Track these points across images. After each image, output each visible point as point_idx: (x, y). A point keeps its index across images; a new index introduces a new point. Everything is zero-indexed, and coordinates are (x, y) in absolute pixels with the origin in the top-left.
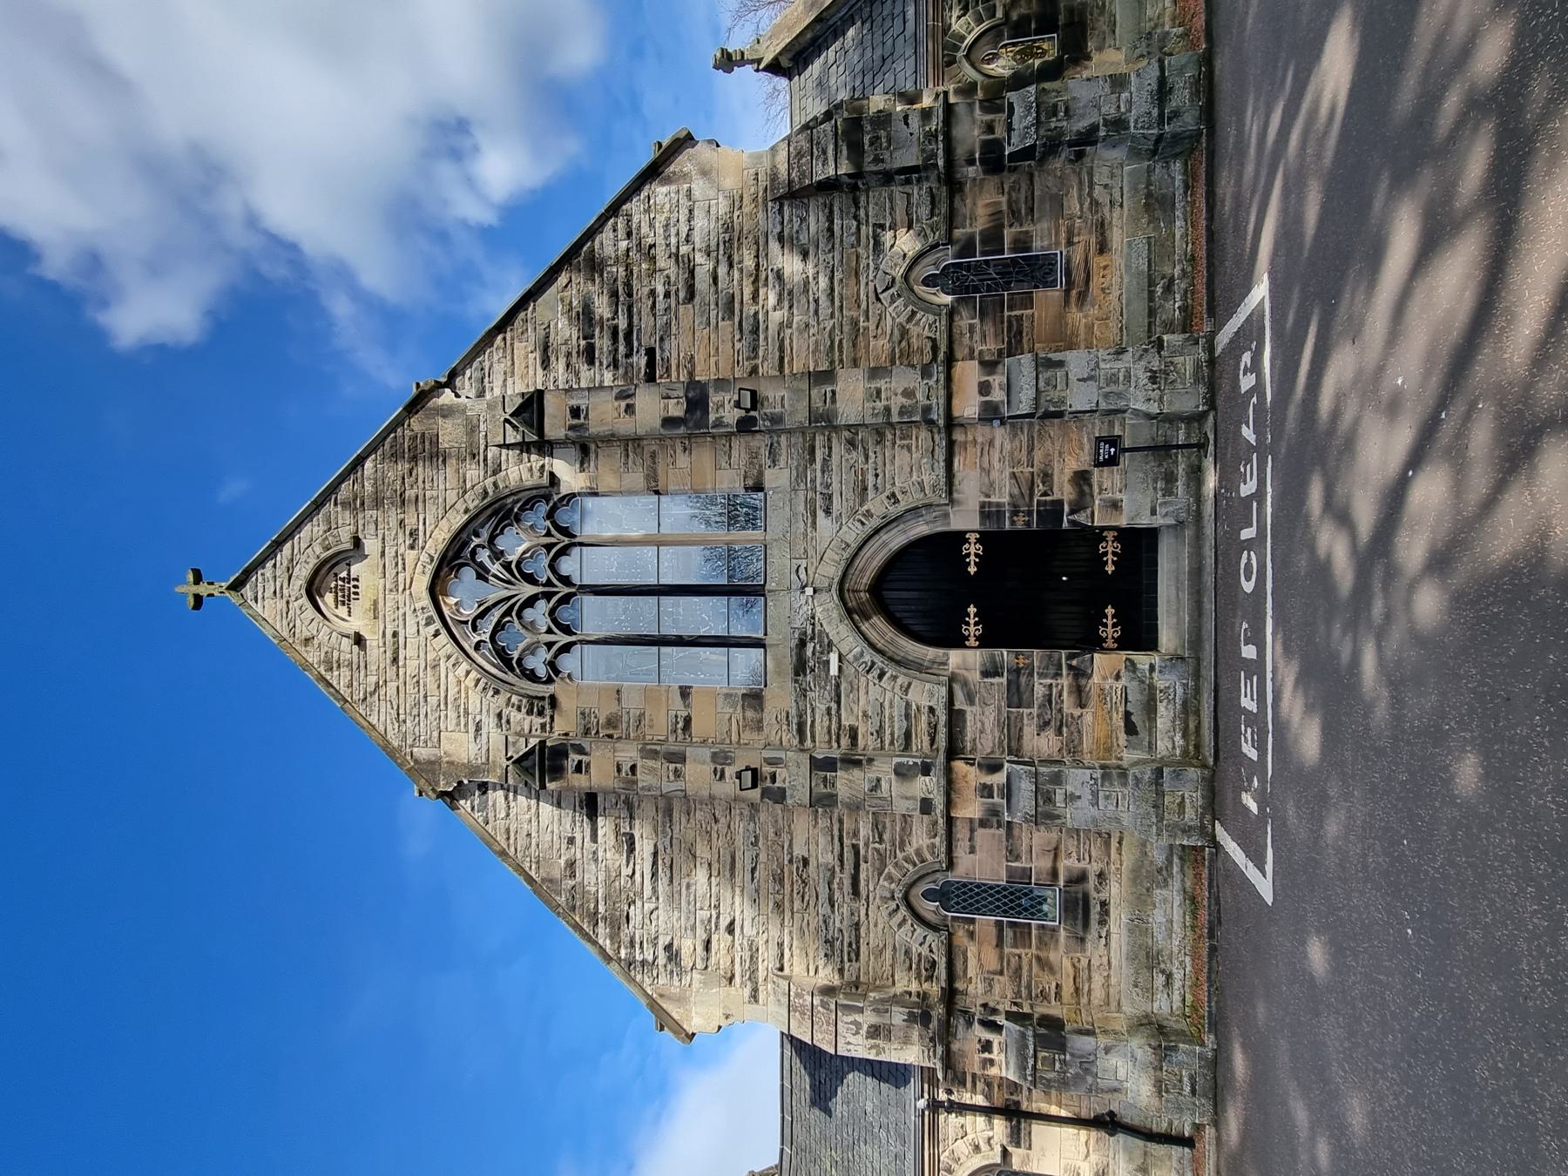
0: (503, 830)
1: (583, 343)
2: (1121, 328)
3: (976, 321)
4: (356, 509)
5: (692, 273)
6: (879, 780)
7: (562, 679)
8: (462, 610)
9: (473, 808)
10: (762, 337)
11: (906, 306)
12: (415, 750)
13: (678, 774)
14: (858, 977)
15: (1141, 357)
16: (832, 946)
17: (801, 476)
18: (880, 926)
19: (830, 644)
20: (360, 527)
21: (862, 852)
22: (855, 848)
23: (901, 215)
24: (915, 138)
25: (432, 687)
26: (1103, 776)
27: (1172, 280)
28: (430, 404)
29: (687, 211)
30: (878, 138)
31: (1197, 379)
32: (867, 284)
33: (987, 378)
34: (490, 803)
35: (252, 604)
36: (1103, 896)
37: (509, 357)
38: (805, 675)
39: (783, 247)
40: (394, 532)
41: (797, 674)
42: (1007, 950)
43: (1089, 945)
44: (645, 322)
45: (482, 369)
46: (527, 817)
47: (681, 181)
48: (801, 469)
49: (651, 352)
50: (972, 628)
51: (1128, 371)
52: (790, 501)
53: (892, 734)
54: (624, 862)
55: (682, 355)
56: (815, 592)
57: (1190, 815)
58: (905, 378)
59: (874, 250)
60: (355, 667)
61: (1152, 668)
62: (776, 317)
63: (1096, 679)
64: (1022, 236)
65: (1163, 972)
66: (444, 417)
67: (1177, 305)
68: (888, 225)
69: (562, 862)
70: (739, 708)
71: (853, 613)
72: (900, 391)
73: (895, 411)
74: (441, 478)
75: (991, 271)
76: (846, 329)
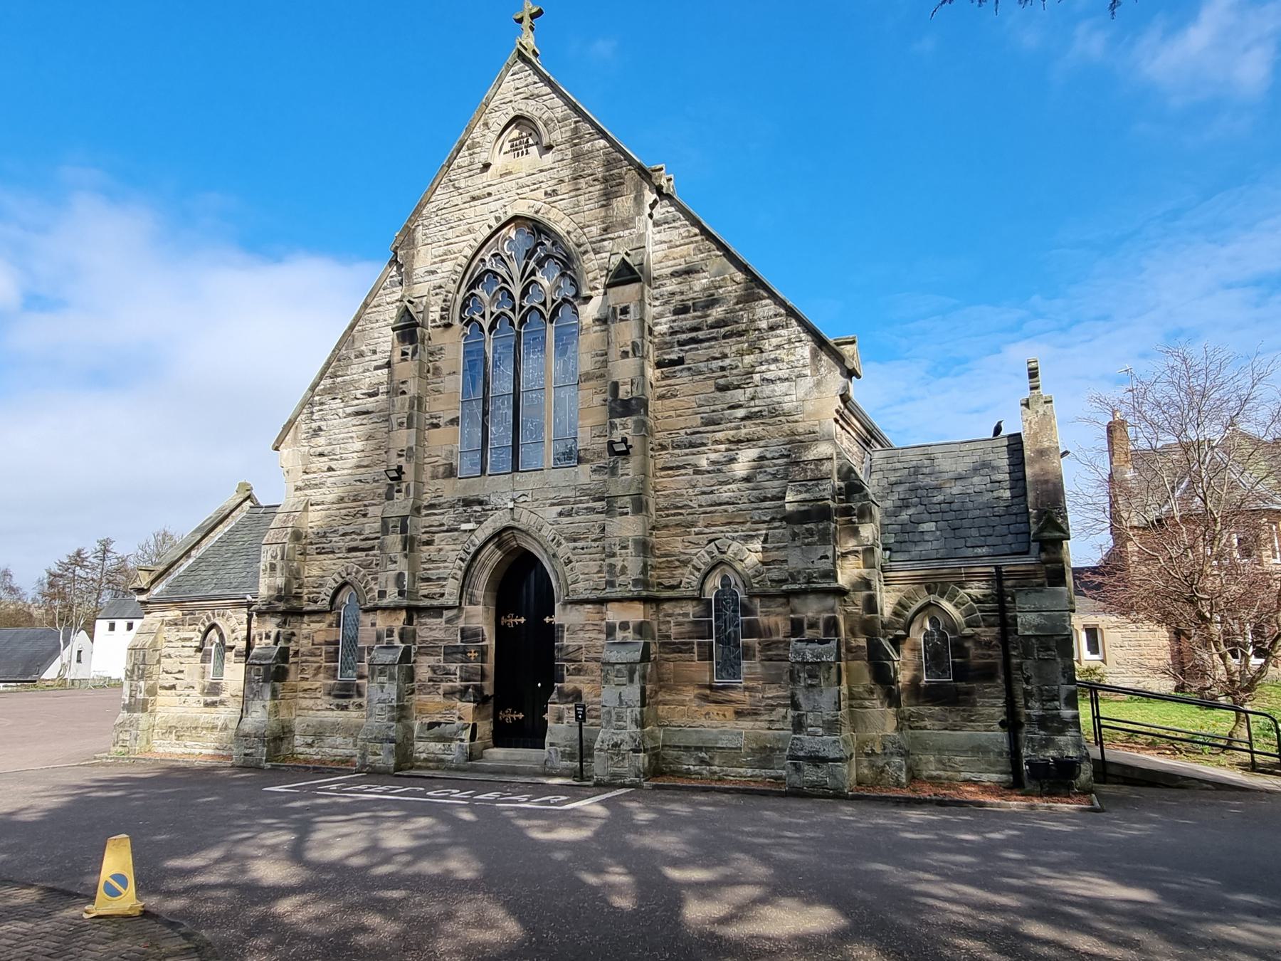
0: (379, 302)
1: (690, 303)
2: (680, 726)
3: (691, 618)
4: (573, 139)
5: (738, 387)
6: (395, 562)
7: (463, 329)
8: (507, 242)
9: (392, 277)
10: (687, 451)
11: (704, 563)
12: (421, 227)
13: (401, 424)
14: (308, 554)
15: (632, 737)
16: (323, 537)
17: (584, 492)
18: (333, 567)
19: (480, 523)
20: (559, 147)
21: (371, 553)
22: (372, 548)
23: (773, 556)
24: (810, 565)
25: (458, 231)
26: (393, 706)
27: (710, 765)
28: (645, 184)
29: (786, 376)
30: (812, 535)
31: (614, 775)
32: (722, 532)
33: (631, 627)
34: (394, 289)
35: (511, 73)
36: (351, 707)
37: (682, 242)
38: (463, 506)
39: (754, 461)
40: (556, 176)
41: (464, 500)
42: (323, 647)
43: (327, 698)
44: (702, 352)
45: (674, 221)
46: (387, 318)
47: (813, 367)
48: (588, 492)
49: (680, 361)
50: (511, 621)
51: (625, 728)
52: (569, 486)
53: (429, 569)
54: (364, 391)
55: (677, 387)
56: (512, 509)
57: (371, 758)
58: (634, 570)
59: (747, 536)
60: (470, 168)
61: (462, 740)
62: (703, 463)
63: (459, 704)
64: (751, 652)
65: (313, 742)
66: (635, 198)
67: (691, 767)
68: (766, 545)
69: (364, 348)
70: (445, 462)
71: (498, 537)
72: (625, 563)
73: (612, 560)
74: (591, 206)
75: (732, 629)
76: (690, 518)
